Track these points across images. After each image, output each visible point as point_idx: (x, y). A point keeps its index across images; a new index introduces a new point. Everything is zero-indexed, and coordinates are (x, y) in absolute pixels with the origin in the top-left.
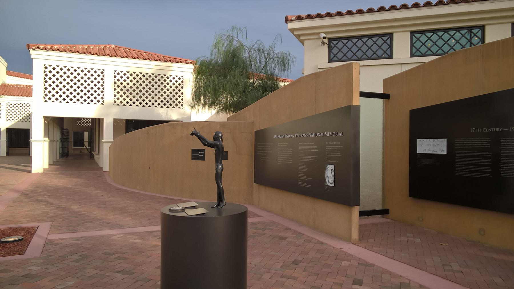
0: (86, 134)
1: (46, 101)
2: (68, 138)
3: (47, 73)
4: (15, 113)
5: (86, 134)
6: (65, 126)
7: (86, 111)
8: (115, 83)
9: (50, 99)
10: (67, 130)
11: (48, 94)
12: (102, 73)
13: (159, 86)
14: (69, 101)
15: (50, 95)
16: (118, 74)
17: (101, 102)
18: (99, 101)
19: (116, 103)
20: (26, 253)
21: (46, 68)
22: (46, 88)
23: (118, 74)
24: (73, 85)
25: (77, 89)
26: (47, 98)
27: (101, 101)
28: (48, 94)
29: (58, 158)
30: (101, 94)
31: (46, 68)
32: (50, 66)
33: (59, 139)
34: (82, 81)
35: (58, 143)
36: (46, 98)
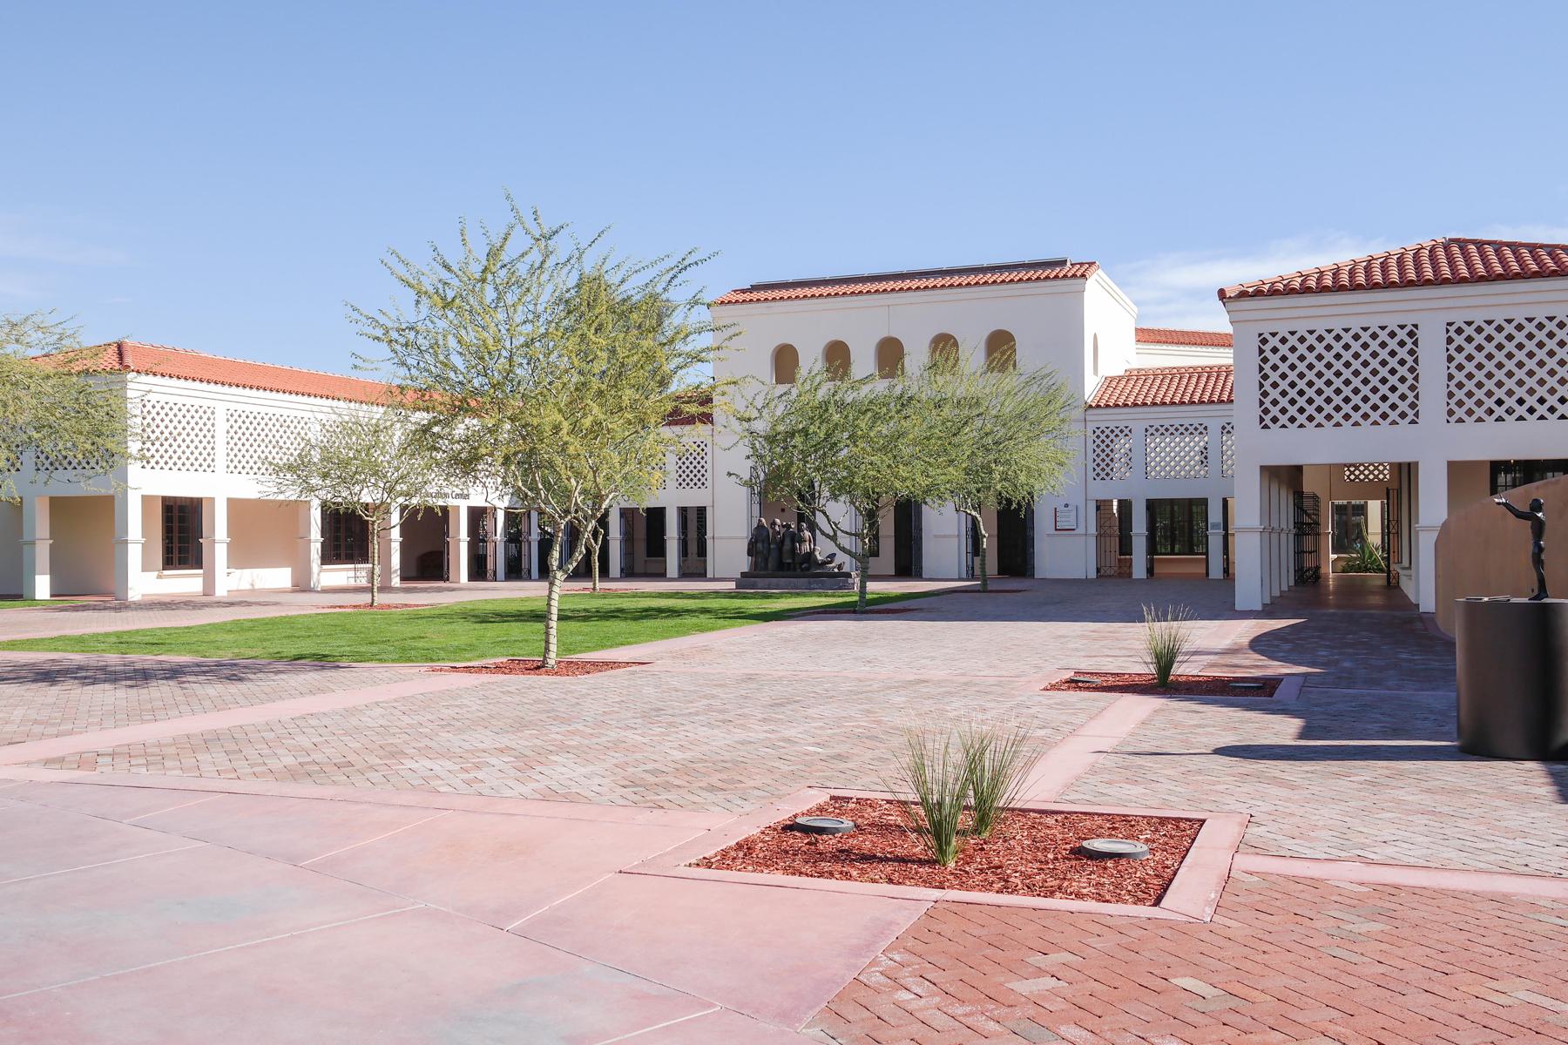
0: (1374, 508)
1: (1266, 427)
2: (1318, 524)
3: (1268, 354)
4: (1541, 373)
5: (1374, 508)
6: (1307, 488)
7: (1365, 445)
8: (1450, 359)
9: (1275, 420)
10: (1315, 498)
11: (1270, 407)
12: (1411, 334)
13: (1310, 366)
14: (1306, 423)
15: (1275, 411)
16: (1459, 331)
17: (1411, 417)
18: (1403, 415)
19: (1455, 417)
20: (1163, 904)
21: (1264, 341)
22: (1265, 394)
23: (1459, 331)
24: (1546, 359)
25: (1546, 359)
26: (1267, 419)
27: (1411, 413)
28: (1270, 407)
29: (1292, 583)
30: (1411, 395)
31: (1264, 341)
32: (1274, 335)
33: (1291, 526)
34: (1301, 367)
35: (1291, 537)
36: (1266, 421)
